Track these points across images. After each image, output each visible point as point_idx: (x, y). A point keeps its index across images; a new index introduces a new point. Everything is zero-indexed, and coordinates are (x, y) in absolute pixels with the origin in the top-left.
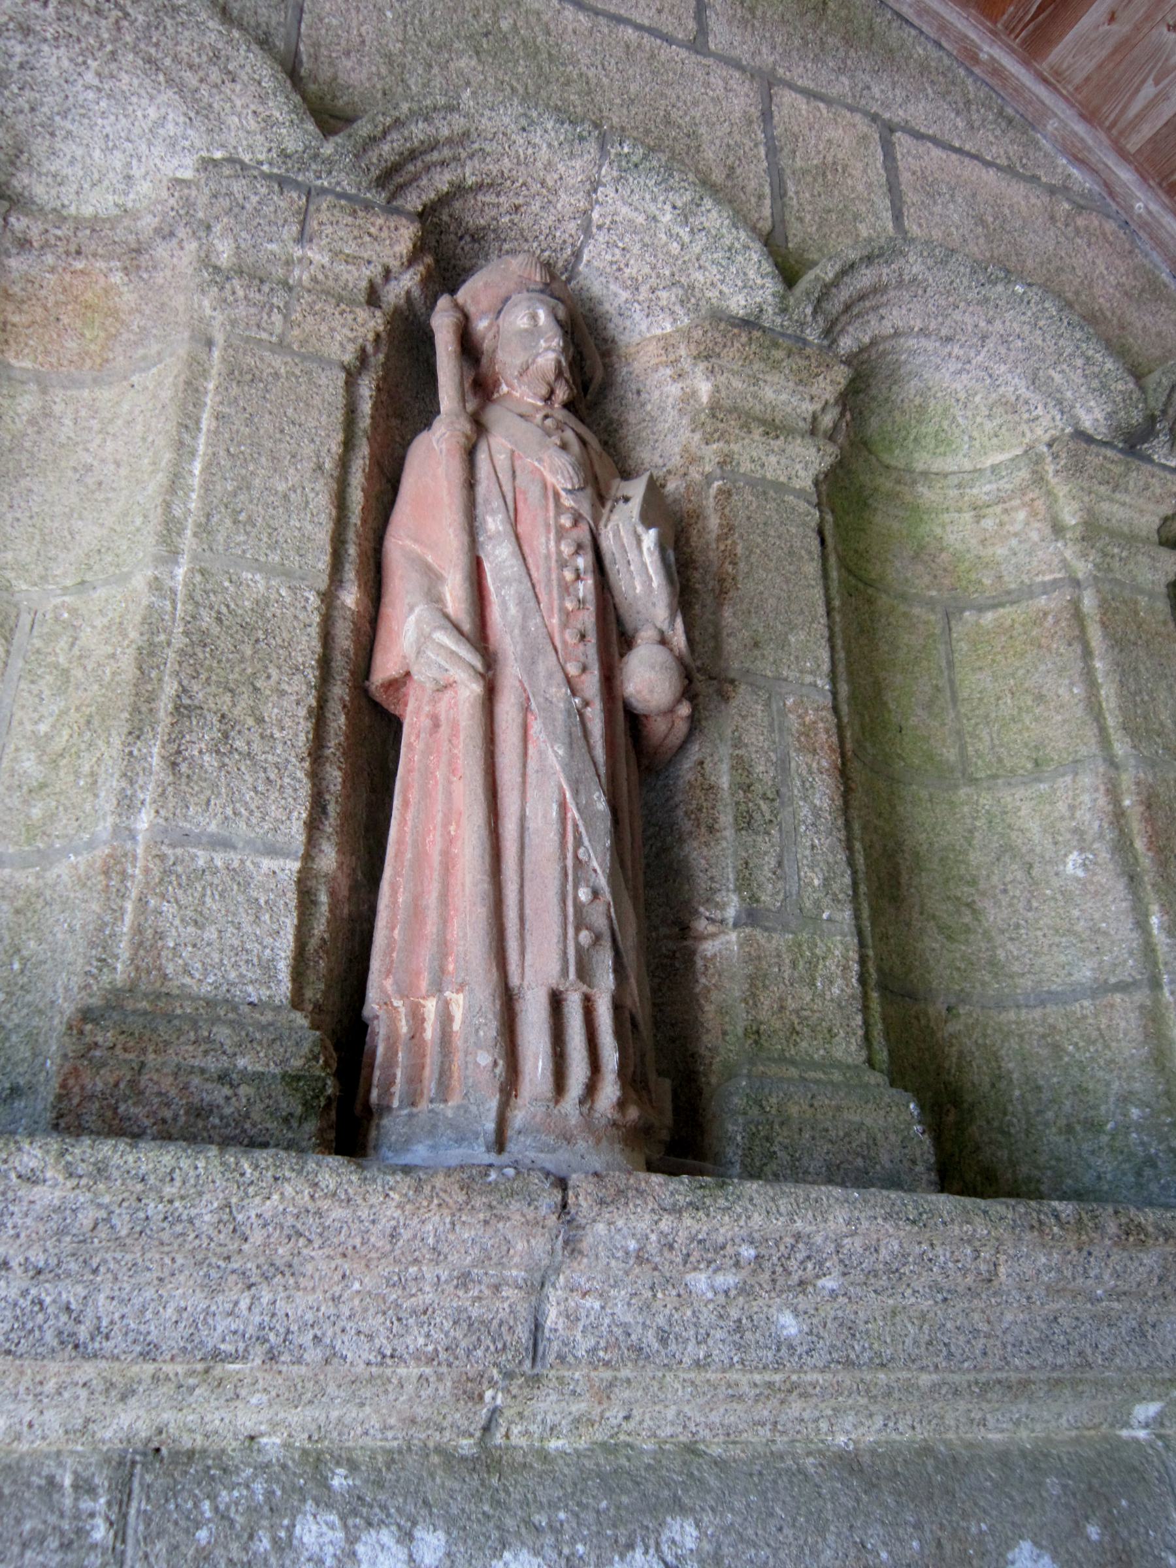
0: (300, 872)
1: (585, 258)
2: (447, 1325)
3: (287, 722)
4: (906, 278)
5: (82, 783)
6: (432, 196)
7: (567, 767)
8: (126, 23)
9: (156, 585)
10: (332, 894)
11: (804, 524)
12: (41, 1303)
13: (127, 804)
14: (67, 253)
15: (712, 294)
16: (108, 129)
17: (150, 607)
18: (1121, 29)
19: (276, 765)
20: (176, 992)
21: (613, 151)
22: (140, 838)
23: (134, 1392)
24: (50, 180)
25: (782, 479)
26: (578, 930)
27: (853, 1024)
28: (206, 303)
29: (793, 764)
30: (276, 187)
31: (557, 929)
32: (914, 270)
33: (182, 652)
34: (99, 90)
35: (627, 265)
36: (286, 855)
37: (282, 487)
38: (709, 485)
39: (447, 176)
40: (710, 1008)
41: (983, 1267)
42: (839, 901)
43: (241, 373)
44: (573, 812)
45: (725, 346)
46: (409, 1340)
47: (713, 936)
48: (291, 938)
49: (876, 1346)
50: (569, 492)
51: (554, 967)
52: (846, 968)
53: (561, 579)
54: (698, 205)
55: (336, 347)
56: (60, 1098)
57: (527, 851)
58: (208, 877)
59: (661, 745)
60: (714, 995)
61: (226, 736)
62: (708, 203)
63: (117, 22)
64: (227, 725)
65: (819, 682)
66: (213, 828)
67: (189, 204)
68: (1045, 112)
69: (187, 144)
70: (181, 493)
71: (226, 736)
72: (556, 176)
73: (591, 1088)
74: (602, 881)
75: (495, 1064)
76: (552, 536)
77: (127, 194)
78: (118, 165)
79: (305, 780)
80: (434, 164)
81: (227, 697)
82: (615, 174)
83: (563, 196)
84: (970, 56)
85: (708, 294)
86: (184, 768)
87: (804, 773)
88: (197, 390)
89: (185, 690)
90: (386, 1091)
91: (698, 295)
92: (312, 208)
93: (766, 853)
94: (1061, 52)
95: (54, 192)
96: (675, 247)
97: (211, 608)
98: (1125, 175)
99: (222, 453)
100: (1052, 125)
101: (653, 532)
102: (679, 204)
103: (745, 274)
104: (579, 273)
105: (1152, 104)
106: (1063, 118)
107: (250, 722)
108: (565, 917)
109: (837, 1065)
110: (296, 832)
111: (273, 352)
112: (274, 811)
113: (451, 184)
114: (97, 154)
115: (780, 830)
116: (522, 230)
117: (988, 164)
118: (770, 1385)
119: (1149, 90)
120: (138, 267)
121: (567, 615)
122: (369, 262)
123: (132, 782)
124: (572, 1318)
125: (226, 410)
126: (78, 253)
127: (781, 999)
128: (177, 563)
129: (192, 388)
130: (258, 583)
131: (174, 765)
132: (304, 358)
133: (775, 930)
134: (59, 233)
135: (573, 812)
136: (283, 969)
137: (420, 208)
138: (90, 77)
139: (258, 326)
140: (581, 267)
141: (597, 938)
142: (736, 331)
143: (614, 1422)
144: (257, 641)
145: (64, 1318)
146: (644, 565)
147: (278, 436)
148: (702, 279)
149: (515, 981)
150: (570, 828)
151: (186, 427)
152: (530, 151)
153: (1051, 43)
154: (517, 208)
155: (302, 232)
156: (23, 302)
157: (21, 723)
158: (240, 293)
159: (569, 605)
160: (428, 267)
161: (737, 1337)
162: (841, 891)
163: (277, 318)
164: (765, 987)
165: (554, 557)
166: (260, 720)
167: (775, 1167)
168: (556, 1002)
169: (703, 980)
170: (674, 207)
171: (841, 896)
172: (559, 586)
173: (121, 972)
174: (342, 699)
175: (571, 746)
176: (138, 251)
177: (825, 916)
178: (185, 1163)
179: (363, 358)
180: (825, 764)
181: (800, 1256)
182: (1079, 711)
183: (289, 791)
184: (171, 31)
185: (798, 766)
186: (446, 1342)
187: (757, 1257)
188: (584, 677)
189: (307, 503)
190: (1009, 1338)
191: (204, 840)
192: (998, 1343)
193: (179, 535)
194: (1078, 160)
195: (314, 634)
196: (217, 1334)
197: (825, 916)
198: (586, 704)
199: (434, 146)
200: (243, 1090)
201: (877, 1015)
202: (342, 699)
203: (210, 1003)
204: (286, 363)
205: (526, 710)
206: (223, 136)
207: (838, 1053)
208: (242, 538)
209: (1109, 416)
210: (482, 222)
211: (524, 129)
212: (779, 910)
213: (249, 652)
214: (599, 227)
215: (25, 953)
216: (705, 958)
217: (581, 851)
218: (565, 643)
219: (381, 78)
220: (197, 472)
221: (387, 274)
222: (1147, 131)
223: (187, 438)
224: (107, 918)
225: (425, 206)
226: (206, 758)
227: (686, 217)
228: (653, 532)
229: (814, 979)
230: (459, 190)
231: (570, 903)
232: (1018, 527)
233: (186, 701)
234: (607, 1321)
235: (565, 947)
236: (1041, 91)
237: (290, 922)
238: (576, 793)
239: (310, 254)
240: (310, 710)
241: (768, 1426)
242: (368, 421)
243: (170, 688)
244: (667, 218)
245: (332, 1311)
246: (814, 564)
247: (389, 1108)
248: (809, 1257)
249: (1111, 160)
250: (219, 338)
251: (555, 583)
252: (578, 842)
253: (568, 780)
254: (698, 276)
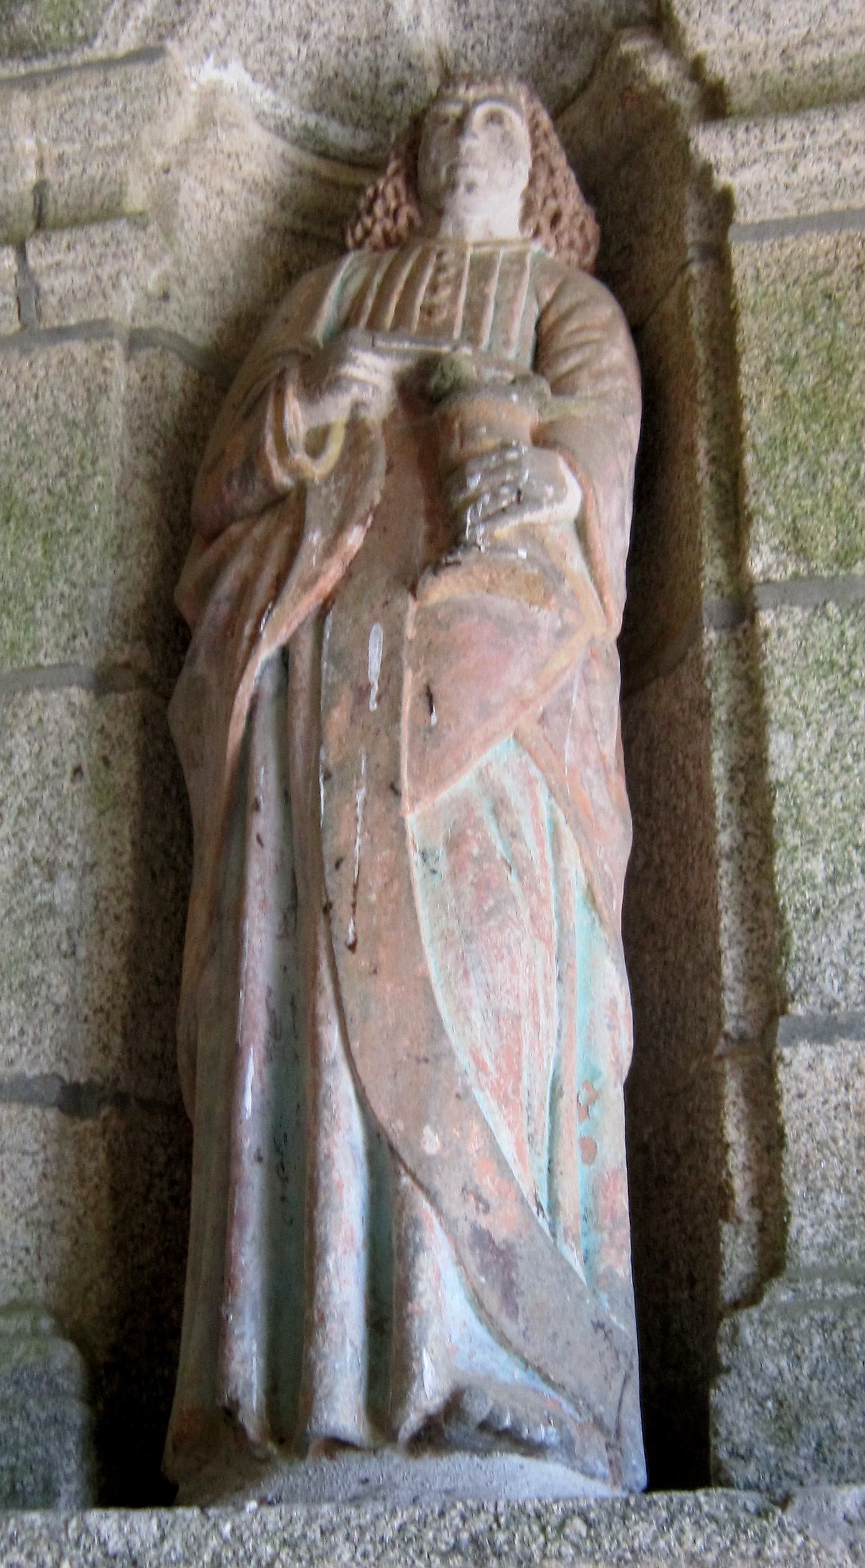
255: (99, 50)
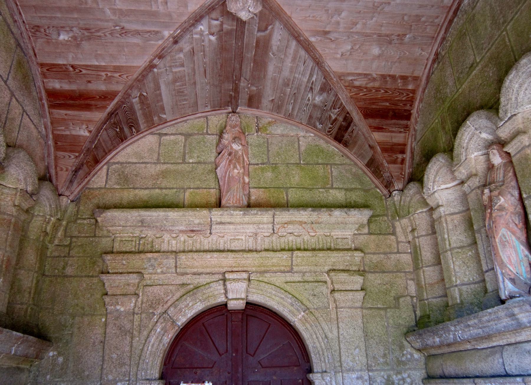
18: (66, 117)
62: (2, 135)
68: (46, 117)
84: (41, 99)
94: (55, 111)
98: (51, 136)
100: (45, 120)
105: (62, 130)
106: (48, 120)
117: (33, 124)
119: (63, 128)
153: (54, 108)
173: (418, 313)
182: (4, 240)
194: (46, 128)
209: (32, 190)
222: (58, 133)
232: (7, 200)
236: (48, 114)
249: (50, 132)
255: (462, 161)
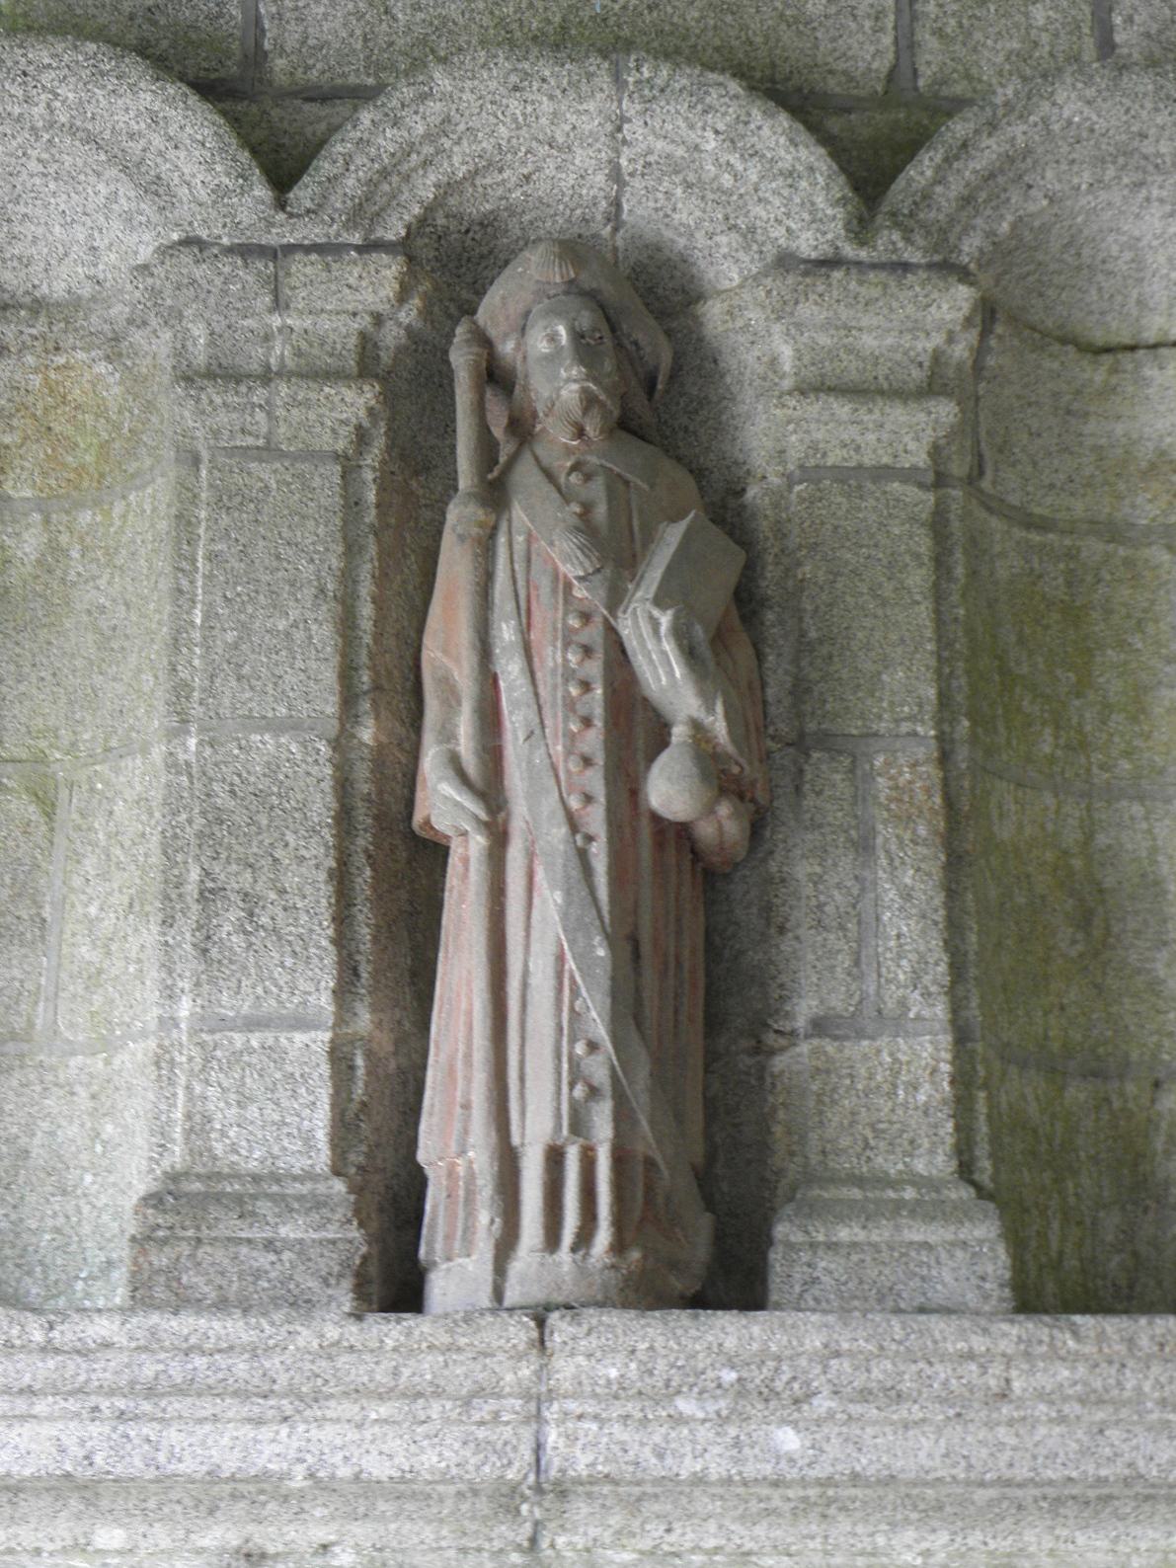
0: (332, 1041)
1: (626, 207)
2: (457, 1446)
3: (308, 889)
4: (1056, 127)
5: (131, 970)
6: (417, 210)
7: (565, 917)
8: (58, 104)
9: (172, 765)
10: (369, 1055)
11: (913, 519)
12: (127, 1436)
13: (170, 994)
14: (46, 351)
15: (778, 232)
16: (62, 207)
17: (168, 785)
19: (300, 937)
20: (226, 1170)
21: (631, 80)
22: (183, 1026)
23: (218, 1508)
24: (15, 263)
25: (886, 460)
26: (572, 1085)
27: (942, 1132)
28: (187, 414)
29: (879, 840)
30: (239, 262)
31: (550, 1087)
32: (1066, 113)
33: (200, 835)
34: (45, 175)
35: (674, 210)
36: (316, 1027)
37: (282, 625)
38: (790, 488)
39: (432, 178)
40: (778, 1130)
41: (993, 1382)
42: (930, 994)
43: (230, 498)
44: (571, 964)
45: (797, 303)
46: (424, 1458)
47: (783, 1049)
48: (327, 1107)
49: (884, 1459)
50: (580, 579)
51: (548, 1125)
52: (934, 1071)
53: (567, 695)
54: (746, 123)
55: (327, 437)
56: (133, 1274)
57: (530, 1008)
58: (246, 1058)
59: (722, 842)
60: (781, 1115)
61: (251, 914)
63: (49, 106)
64: (250, 902)
65: (920, 729)
66: (246, 1009)
67: (155, 293)
69: (143, 219)
70: (184, 650)
71: (251, 914)
72: (567, 128)
73: (584, 1237)
74: (601, 1032)
75: (492, 1222)
76: (559, 644)
77: (95, 265)
78: (81, 237)
79: (331, 948)
80: (414, 170)
81: (248, 875)
82: (638, 107)
83: (579, 151)
85: (774, 234)
86: (214, 952)
87: (893, 847)
88: (189, 523)
89: (208, 874)
90: (431, 1250)
91: (759, 238)
92: (281, 274)
93: (839, 951)
95: (22, 274)
96: (727, 180)
97: (224, 780)
99: (219, 600)
101: (670, 613)
102: (721, 127)
103: (813, 204)
104: (624, 223)
107: (273, 896)
108: (559, 1074)
109: (917, 1181)
110: (324, 1002)
111: (261, 461)
112: (303, 985)
113: (437, 186)
114: (57, 229)
115: (859, 923)
116: (540, 200)
118: (805, 1499)
120: (120, 355)
121: (571, 738)
122: (355, 314)
123: (170, 972)
124: (571, 1439)
125: (219, 547)
126: (57, 349)
127: (853, 1114)
128: (188, 732)
129: (184, 521)
130: (265, 743)
131: (205, 951)
132: (296, 458)
133: (847, 1038)
134: (34, 331)
135: (571, 964)
136: (322, 1136)
137: (403, 233)
138: (34, 166)
139: (243, 431)
140: (624, 216)
141: (593, 1092)
142: (808, 280)
143: (656, 1534)
144: (272, 808)
145: (146, 1447)
146: (664, 653)
147: (275, 564)
148: (763, 214)
149: (516, 1140)
150: (566, 982)
151: (182, 570)
152: (529, 109)
154: (527, 178)
155: (276, 300)
156: (11, 416)
157: (73, 906)
158: (218, 400)
159: (574, 727)
160: (425, 296)
161: (734, 1452)
162: (935, 982)
163: (260, 416)
164: (834, 1102)
165: (560, 670)
166: (282, 892)
167: (817, 1293)
168: (555, 1158)
169: (771, 1099)
170: (717, 132)
171: (933, 989)
172: (565, 705)
174: (366, 851)
175: (568, 893)
176: (116, 339)
177: (911, 1015)
178: (216, 1325)
179: (362, 437)
180: (922, 831)
181: (785, 1378)
183: (316, 960)
184: (103, 103)
185: (887, 840)
186: (455, 1460)
187: (739, 1380)
188: (589, 809)
189: (310, 637)
190: (1042, 1451)
191: (239, 1022)
192: (1028, 1456)
193: (187, 698)
195: (328, 790)
196: (265, 1456)
197: (911, 1015)
198: (589, 839)
199: (410, 148)
200: (287, 1256)
201: (982, 1118)
202: (366, 851)
203: (256, 1179)
204: (275, 471)
205: (530, 856)
206: (176, 213)
207: (920, 1166)
208: (248, 695)
210: (488, 207)
211: (516, 88)
212: (853, 1014)
213: (264, 822)
214: (631, 175)
215: (104, 1136)
216: (772, 1076)
217: (578, 1004)
218: (568, 772)
219: (360, 17)
220: (198, 621)
221: (378, 319)
223: (185, 583)
224: (163, 1107)
225: (408, 227)
226: (234, 938)
227: (732, 141)
228: (670, 613)
229: (895, 1086)
230: (449, 187)
231: (565, 1059)
233: (210, 885)
234: (605, 1440)
235: (559, 1104)
237: (324, 1096)
238: (572, 942)
239: (289, 321)
240: (331, 873)
241: (819, 1540)
242: (373, 512)
243: (194, 874)
244: (711, 144)
245: (357, 1436)
246: (924, 571)
247: (435, 1264)
248: (794, 1378)
250: (205, 455)
251: (560, 702)
252: (575, 993)
253: (565, 931)
254: (758, 210)
